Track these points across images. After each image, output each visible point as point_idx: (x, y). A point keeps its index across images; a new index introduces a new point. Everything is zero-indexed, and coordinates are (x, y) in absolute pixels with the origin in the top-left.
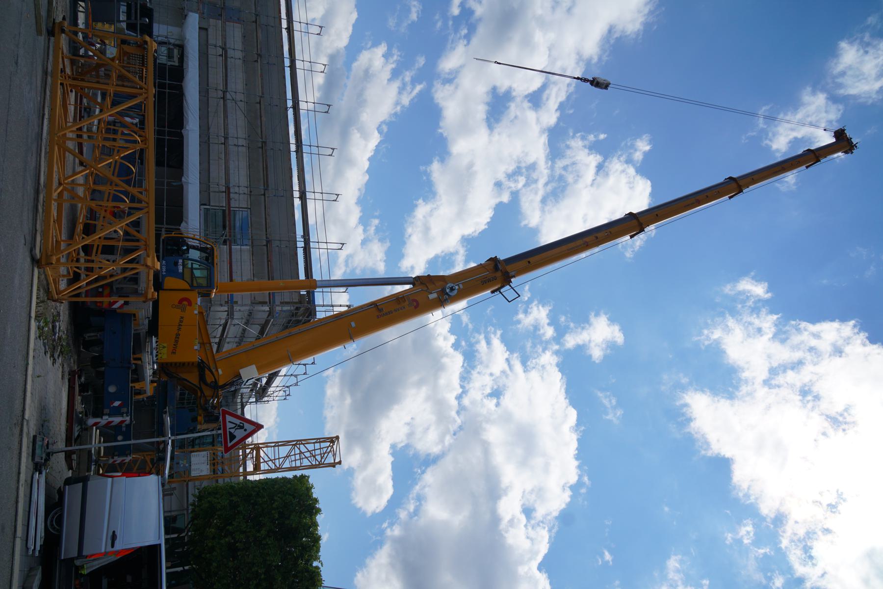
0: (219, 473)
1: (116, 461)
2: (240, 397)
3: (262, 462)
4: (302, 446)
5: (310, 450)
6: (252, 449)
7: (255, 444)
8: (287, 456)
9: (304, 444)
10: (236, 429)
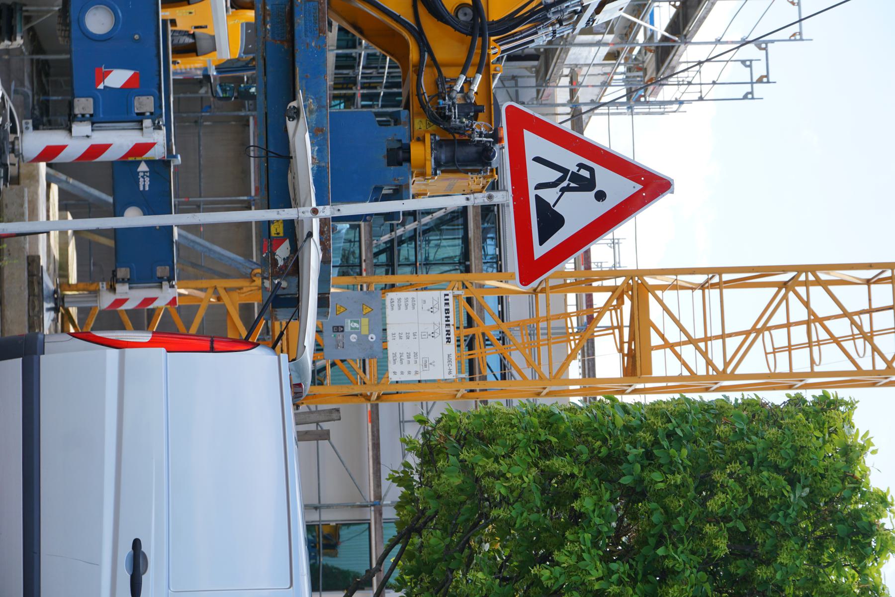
0: (490, 377)
1: (122, 301)
2: (565, 81)
3: (658, 347)
4: (817, 292)
5: (850, 310)
6: (618, 294)
7: (630, 274)
8: (758, 330)
9: (825, 284)
10: (563, 190)
